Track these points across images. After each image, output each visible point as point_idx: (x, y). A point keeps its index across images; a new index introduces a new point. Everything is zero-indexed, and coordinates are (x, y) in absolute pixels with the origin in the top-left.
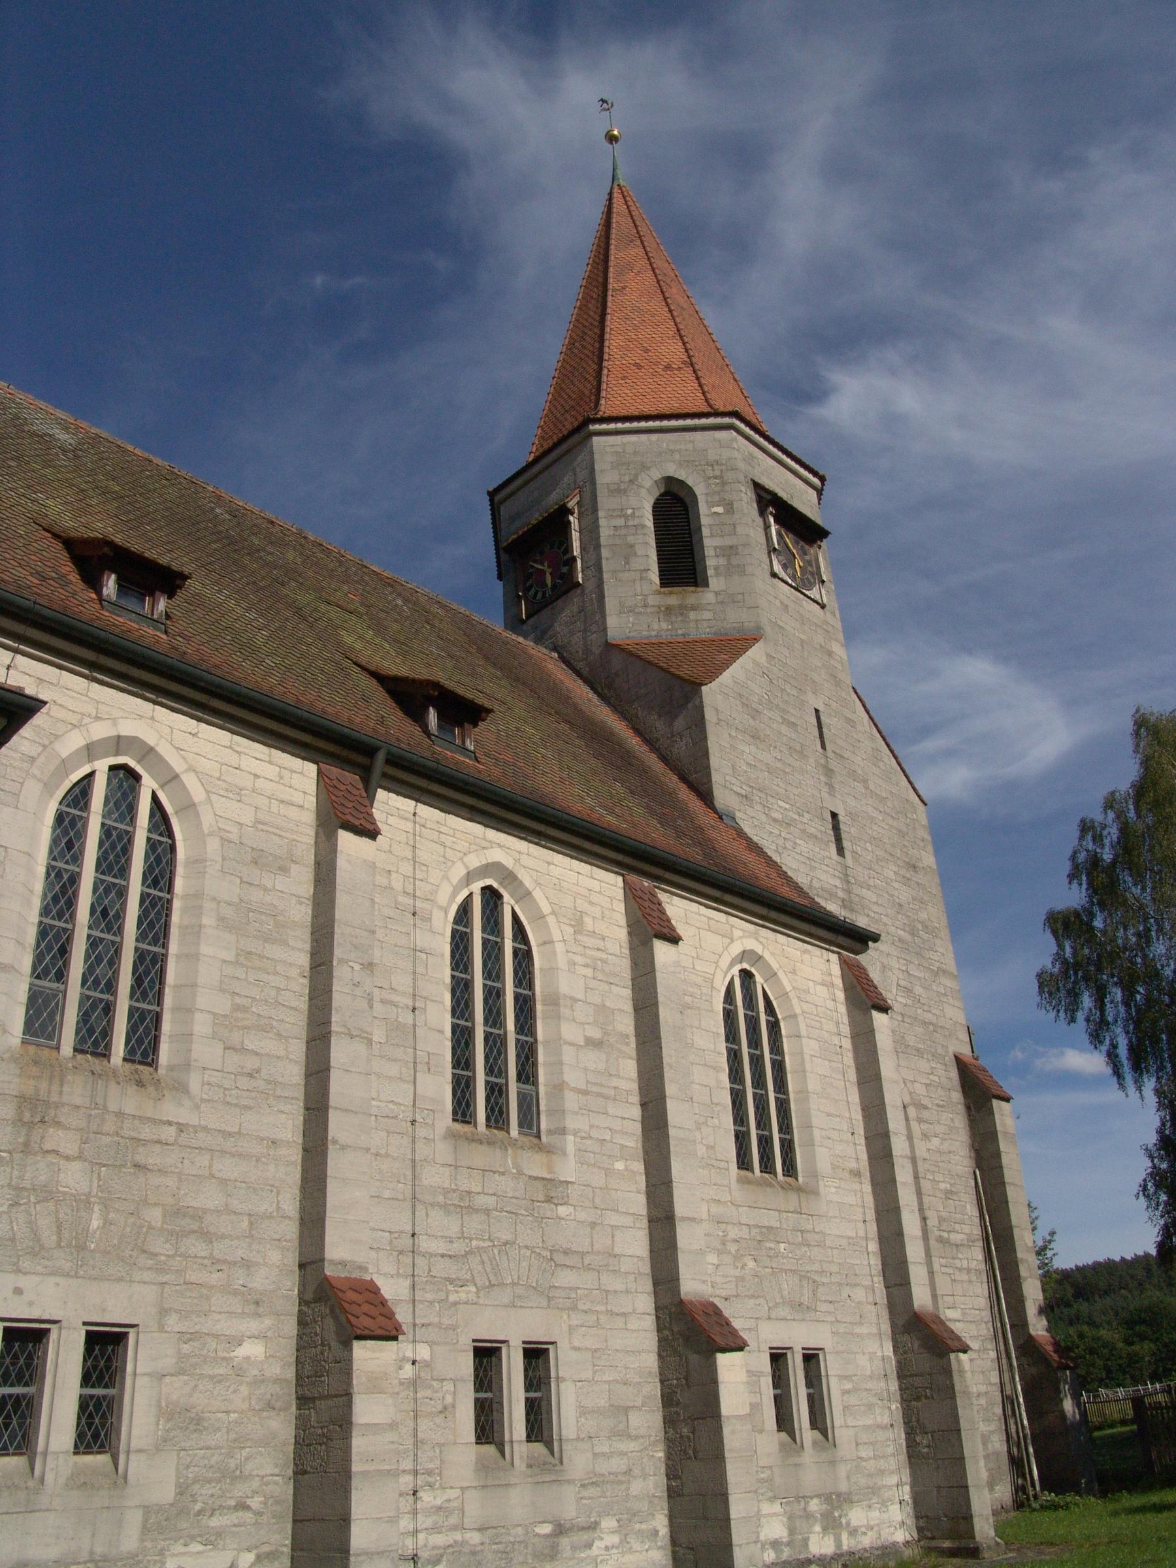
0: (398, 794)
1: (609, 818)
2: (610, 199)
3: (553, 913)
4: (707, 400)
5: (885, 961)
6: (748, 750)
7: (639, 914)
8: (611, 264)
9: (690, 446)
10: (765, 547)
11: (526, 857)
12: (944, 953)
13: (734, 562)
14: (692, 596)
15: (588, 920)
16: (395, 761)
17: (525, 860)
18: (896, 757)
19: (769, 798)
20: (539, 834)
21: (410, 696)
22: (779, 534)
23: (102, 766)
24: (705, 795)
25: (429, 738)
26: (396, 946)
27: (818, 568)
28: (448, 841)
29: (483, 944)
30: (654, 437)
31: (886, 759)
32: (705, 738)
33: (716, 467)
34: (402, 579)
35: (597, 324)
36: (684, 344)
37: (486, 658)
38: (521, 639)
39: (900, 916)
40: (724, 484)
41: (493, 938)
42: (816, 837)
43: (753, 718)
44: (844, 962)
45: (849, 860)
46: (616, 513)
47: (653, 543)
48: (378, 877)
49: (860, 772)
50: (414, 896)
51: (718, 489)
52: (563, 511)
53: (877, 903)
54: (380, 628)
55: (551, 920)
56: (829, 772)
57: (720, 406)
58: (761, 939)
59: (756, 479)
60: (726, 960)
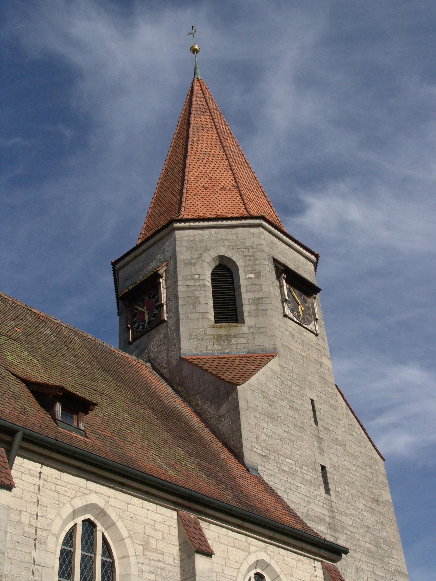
0: (30, 459)
1: (172, 473)
2: (192, 87)
3: (130, 537)
4: (246, 209)
5: (358, 565)
6: (267, 426)
7: (187, 537)
8: (191, 125)
9: (235, 237)
10: (280, 298)
11: (113, 499)
12: (398, 559)
13: (261, 307)
14: (234, 329)
15: (153, 541)
16: (26, 438)
17: (112, 502)
18: (364, 430)
19: (281, 458)
20: (123, 485)
21: (45, 395)
22: (289, 290)
23: (79, 520)
24: (238, 455)
25: (55, 422)
26: (21, 561)
27: (314, 311)
28: (61, 489)
29: (82, 559)
30: (213, 231)
31: (357, 431)
32: (238, 418)
33: (250, 250)
34: (52, 317)
35: (181, 161)
36: (234, 174)
37: (103, 368)
38: (127, 355)
39: (368, 534)
40: (255, 260)
41: (89, 554)
42: (311, 482)
43: (270, 406)
44: (325, 568)
45: (333, 497)
46: (188, 278)
47: (211, 296)
48: (12, 515)
49: (340, 439)
50: (36, 527)
51: (251, 263)
52: (156, 276)
53: (352, 525)
54: (33, 350)
55: (128, 542)
56: (320, 440)
57: (254, 212)
58: (269, 552)
59: (275, 257)
60: (245, 567)
